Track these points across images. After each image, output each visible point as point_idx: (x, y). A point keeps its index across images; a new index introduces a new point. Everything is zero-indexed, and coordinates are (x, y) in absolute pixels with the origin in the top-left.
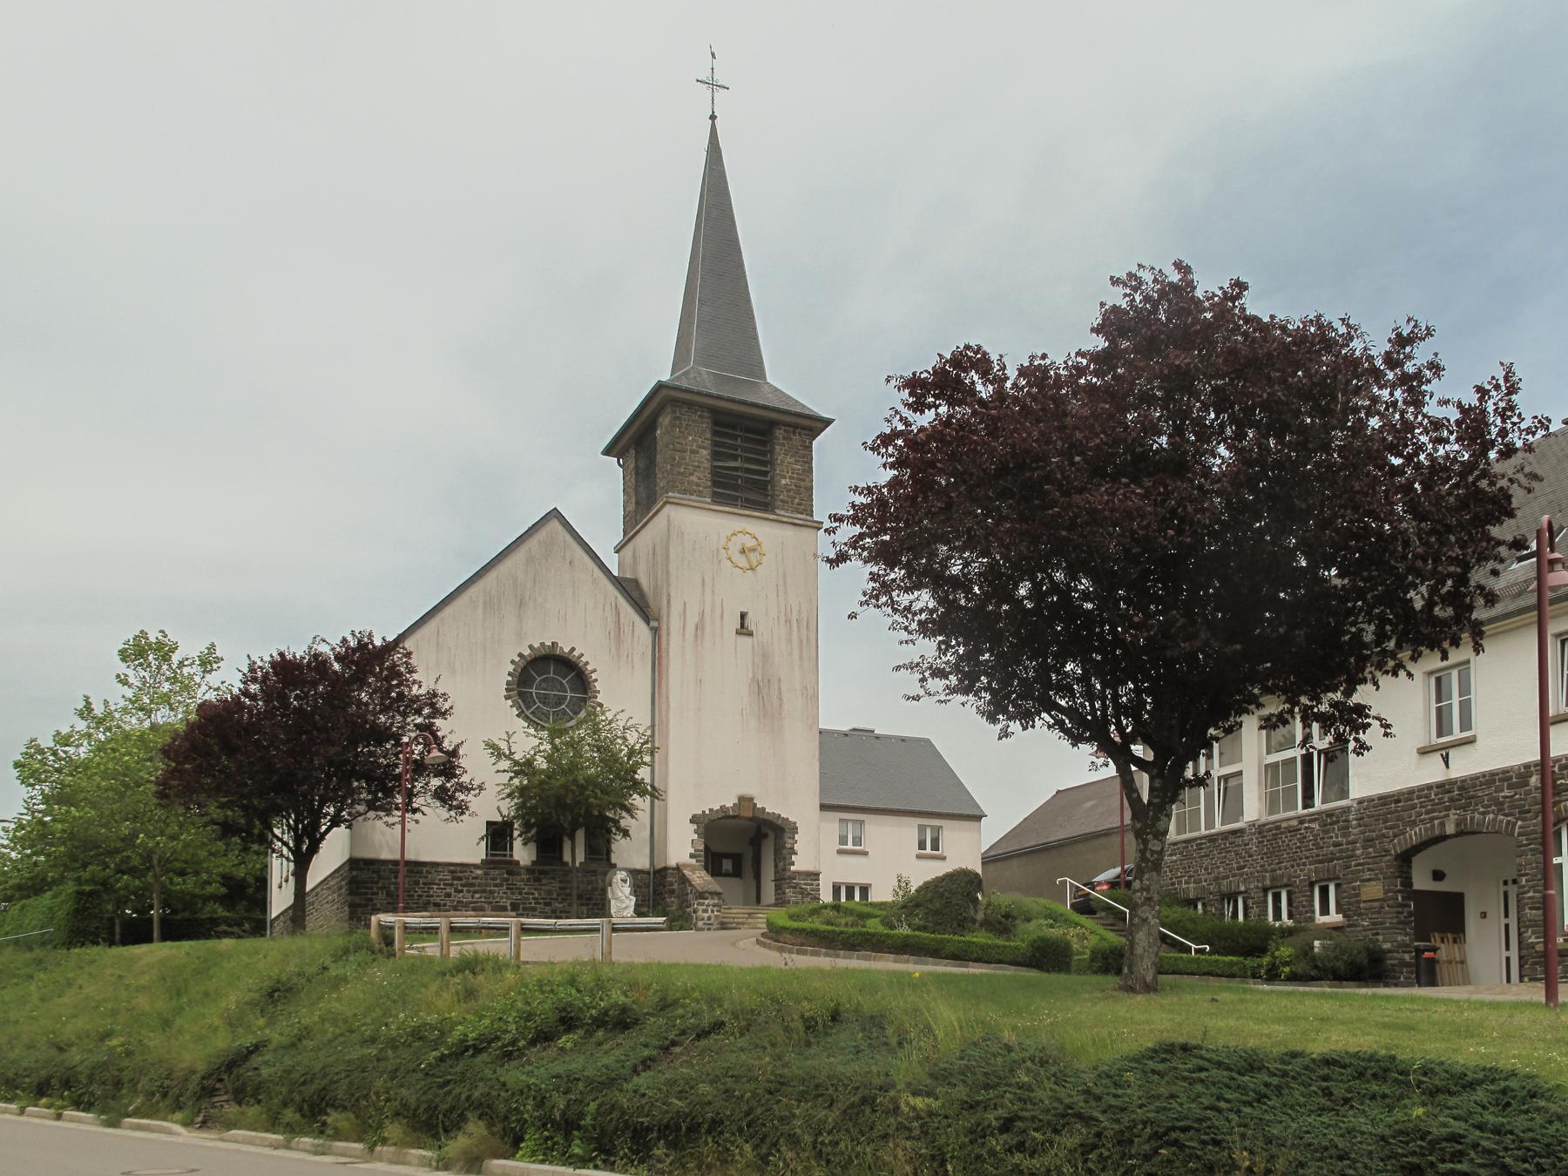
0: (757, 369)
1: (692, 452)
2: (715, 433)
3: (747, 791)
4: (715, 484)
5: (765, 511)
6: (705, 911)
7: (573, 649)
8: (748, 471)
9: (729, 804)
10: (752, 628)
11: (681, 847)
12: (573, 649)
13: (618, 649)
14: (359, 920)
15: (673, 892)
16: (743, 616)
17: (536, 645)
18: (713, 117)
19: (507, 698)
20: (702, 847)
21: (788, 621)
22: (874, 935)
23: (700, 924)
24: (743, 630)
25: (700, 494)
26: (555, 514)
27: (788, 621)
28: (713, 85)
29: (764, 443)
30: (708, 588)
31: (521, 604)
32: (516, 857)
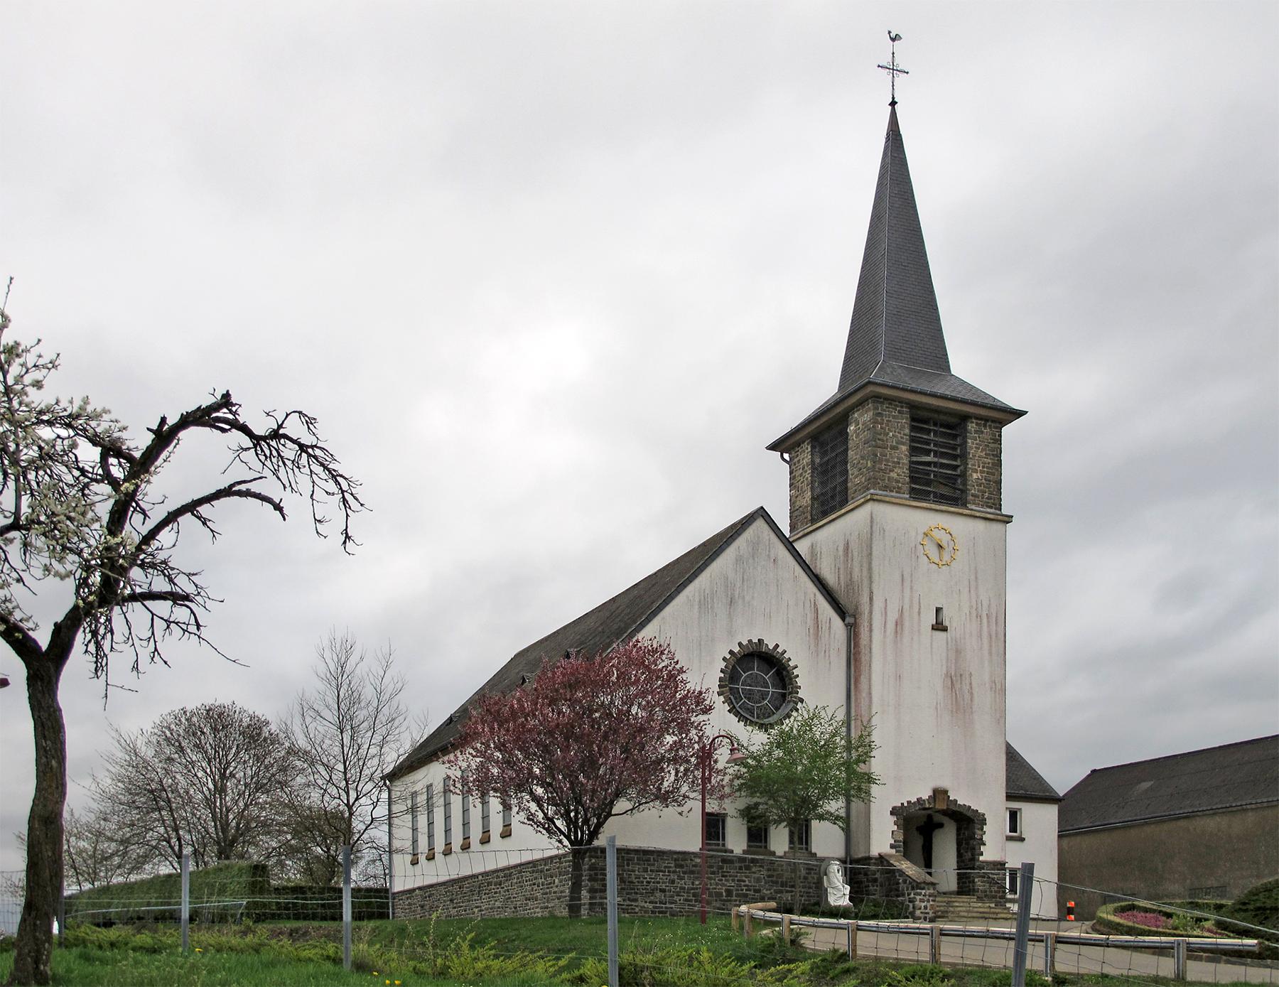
0: (940, 361)
1: (893, 448)
2: (913, 428)
3: (943, 783)
4: (913, 479)
5: (956, 505)
6: (922, 901)
7: (777, 646)
8: (943, 466)
9: (925, 797)
10: (946, 623)
11: (882, 838)
12: (777, 646)
13: (817, 645)
14: (71, 905)
15: (875, 880)
16: (938, 610)
18: (893, 104)
21: (979, 616)
23: (918, 913)
24: (939, 627)
26: (761, 513)
27: (979, 616)
28: (893, 70)
29: (955, 437)
30: (907, 584)
31: (732, 602)
32: (729, 846)
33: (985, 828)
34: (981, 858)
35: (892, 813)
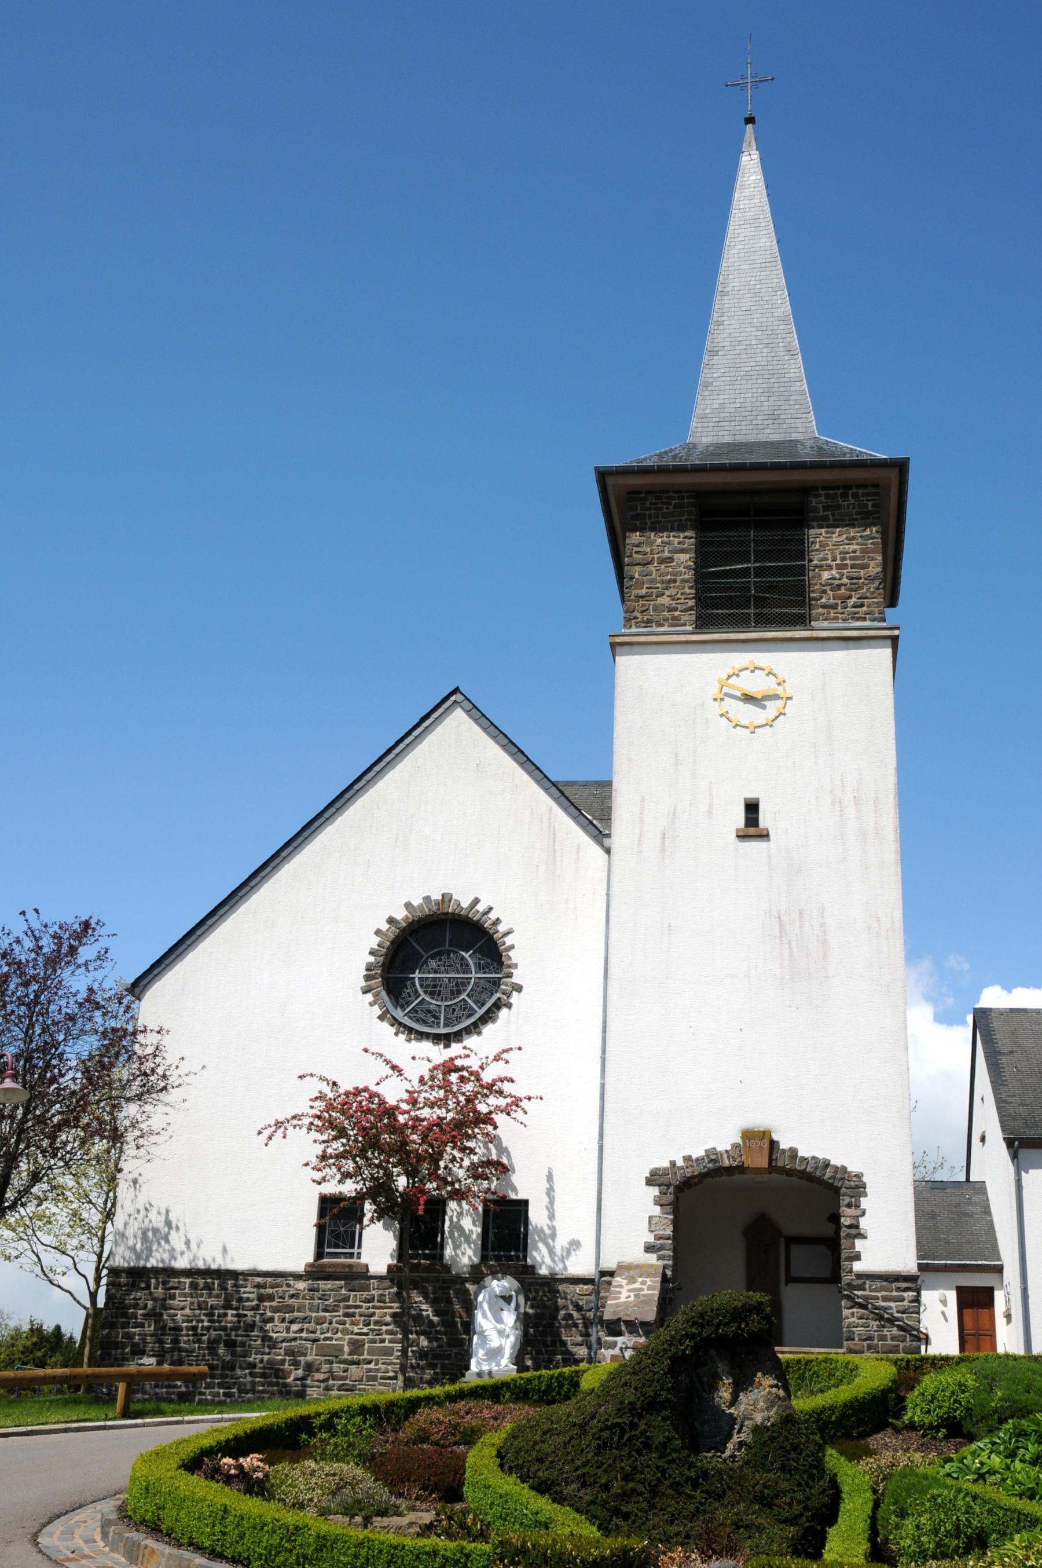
1: (662, 561)
3: (757, 1121)
7: (476, 901)
17: (416, 902)
19: (365, 991)
20: (669, 1231)
22: (477, 1387)
25: (675, 621)
33: (864, 1203)
34: (857, 1267)
35: (649, 1182)
